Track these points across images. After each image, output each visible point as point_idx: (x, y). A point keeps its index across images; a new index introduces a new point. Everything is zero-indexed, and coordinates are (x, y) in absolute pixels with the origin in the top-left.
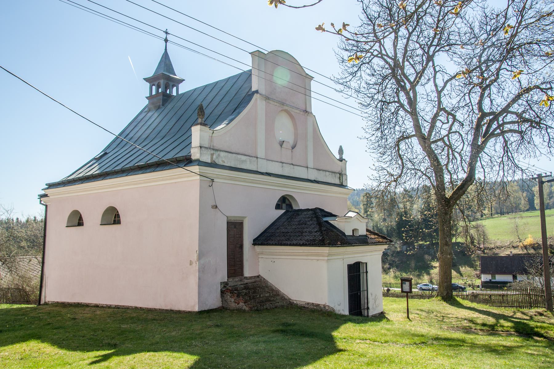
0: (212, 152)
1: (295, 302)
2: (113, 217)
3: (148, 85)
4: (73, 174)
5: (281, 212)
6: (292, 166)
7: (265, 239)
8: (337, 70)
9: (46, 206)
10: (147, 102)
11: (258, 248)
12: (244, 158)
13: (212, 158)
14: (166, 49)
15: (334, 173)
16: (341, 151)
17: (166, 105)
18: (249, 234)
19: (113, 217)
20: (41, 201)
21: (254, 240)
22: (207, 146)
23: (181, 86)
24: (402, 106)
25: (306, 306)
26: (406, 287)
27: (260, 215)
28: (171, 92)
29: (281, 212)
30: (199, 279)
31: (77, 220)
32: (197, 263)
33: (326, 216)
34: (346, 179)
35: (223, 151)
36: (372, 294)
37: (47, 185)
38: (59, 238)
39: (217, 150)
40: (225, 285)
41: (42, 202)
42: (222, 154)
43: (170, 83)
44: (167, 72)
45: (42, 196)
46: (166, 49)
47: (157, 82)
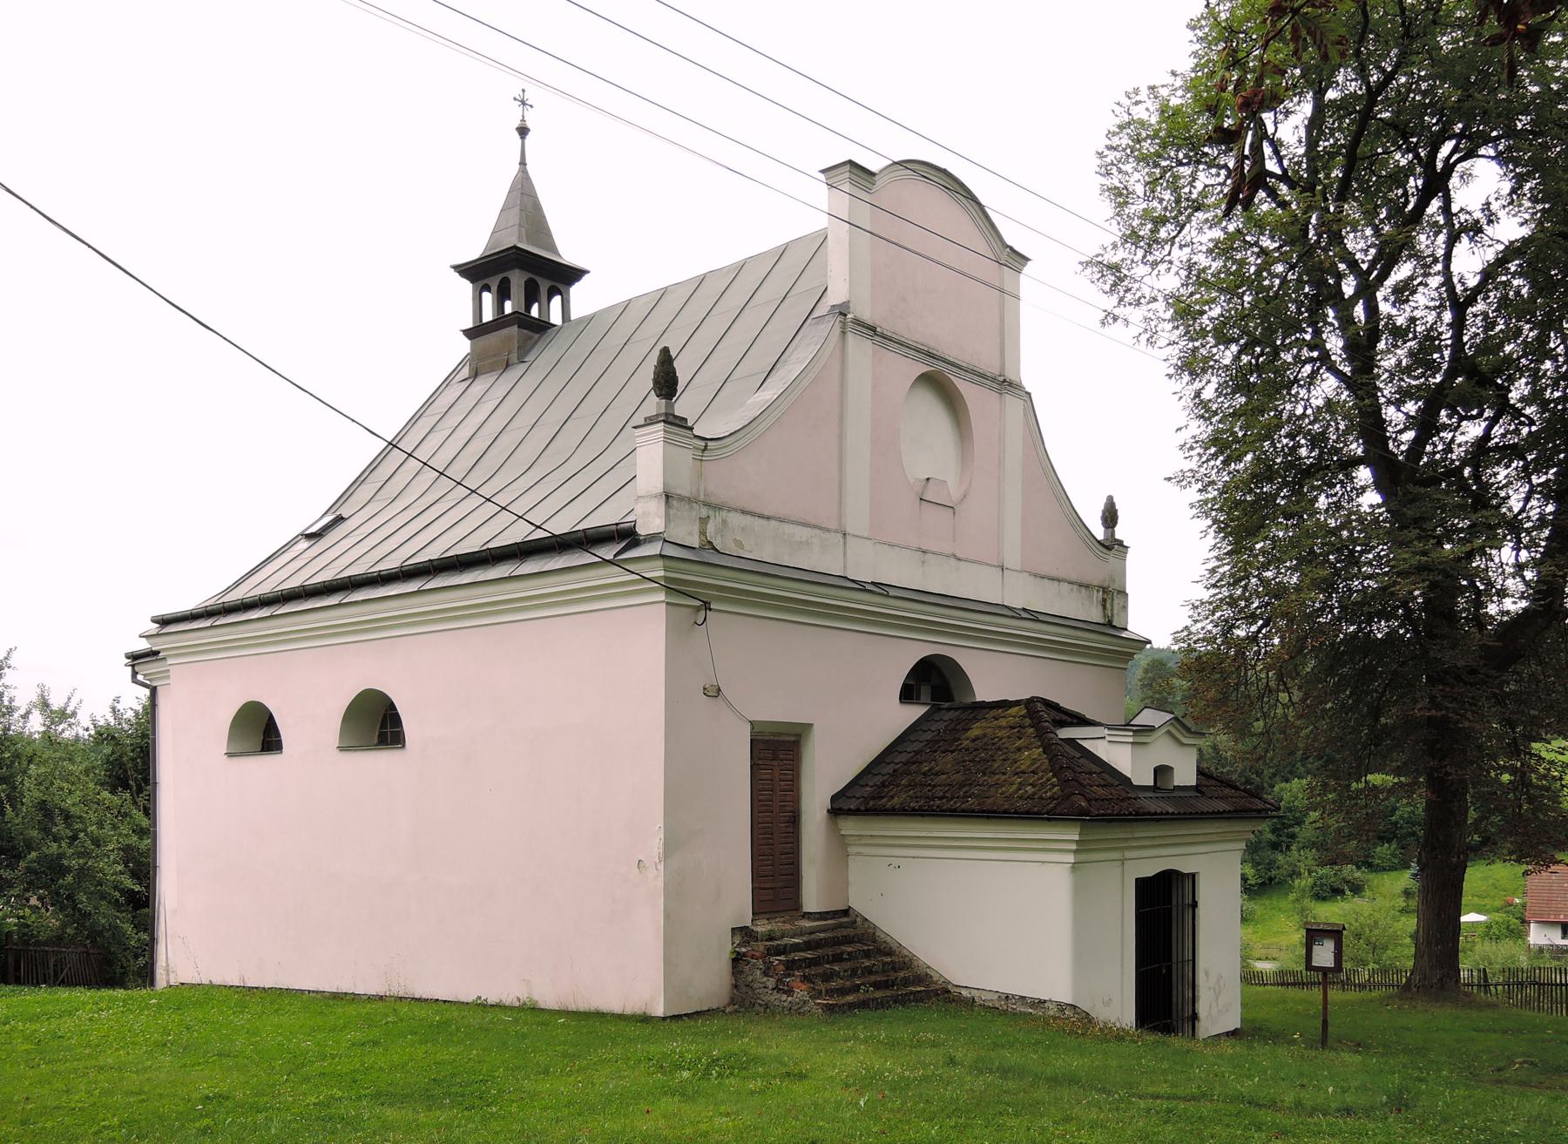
0: (704, 512)
1: (965, 993)
2: (376, 722)
3: (467, 286)
4: (237, 584)
5: (915, 712)
6: (953, 561)
7: (865, 799)
8: (1100, 230)
9: (154, 690)
10: (465, 346)
11: (849, 826)
12: (802, 533)
13: (703, 533)
14: (523, 163)
15: (1087, 587)
16: (1110, 517)
17: (529, 358)
18: (825, 773)
19: (376, 722)
20: (135, 674)
21: (834, 798)
22: (686, 493)
23: (576, 290)
24: (1325, 357)
25: (1002, 1005)
26: (1324, 955)
27: (856, 714)
28: (545, 310)
29: (915, 712)
30: (667, 916)
31: (259, 731)
32: (661, 867)
33: (1062, 724)
34: (1125, 608)
35: (736, 510)
36: (1207, 974)
37: (154, 620)
38: (196, 786)
39: (718, 508)
40: (743, 934)
41: (140, 677)
42: (735, 519)
43: (539, 280)
44: (529, 242)
45: (135, 658)
46: (523, 163)
47: (500, 277)
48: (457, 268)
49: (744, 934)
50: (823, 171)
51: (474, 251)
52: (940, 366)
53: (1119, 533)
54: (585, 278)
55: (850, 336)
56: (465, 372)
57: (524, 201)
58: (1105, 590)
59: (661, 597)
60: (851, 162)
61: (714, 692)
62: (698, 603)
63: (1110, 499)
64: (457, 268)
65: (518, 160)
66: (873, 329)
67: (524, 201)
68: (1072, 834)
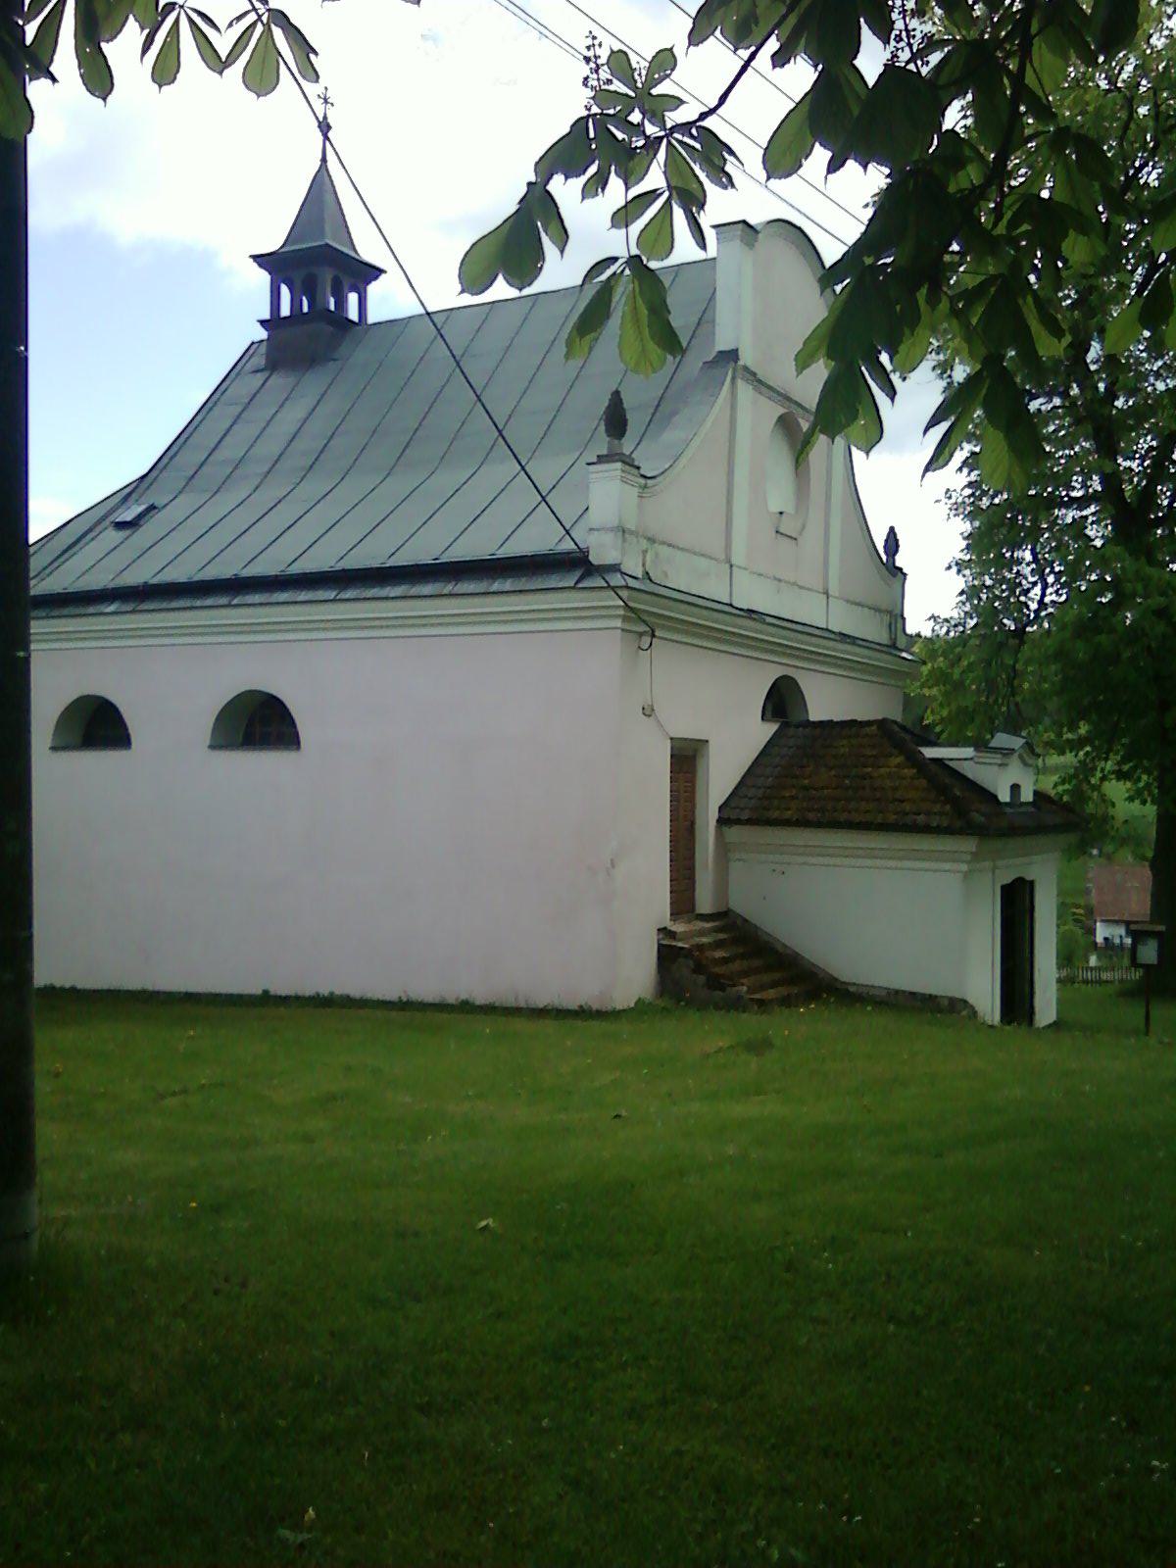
1: (852, 989)
2: (259, 722)
3: (263, 278)
10: (262, 334)
11: (734, 833)
19: (259, 722)
23: (373, 289)
36: (1039, 970)
42: (664, 550)
48: (255, 258)
49: (663, 931)
50: (714, 227)
51: (273, 242)
52: (794, 409)
53: (899, 561)
54: (383, 277)
55: (740, 383)
56: (259, 361)
57: (320, 199)
58: (890, 613)
59: (618, 623)
60: (744, 222)
61: (648, 712)
62: (643, 628)
63: (892, 529)
64: (255, 258)
65: (320, 156)
66: (754, 374)
67: (320, 199)
68: (969, 844)
